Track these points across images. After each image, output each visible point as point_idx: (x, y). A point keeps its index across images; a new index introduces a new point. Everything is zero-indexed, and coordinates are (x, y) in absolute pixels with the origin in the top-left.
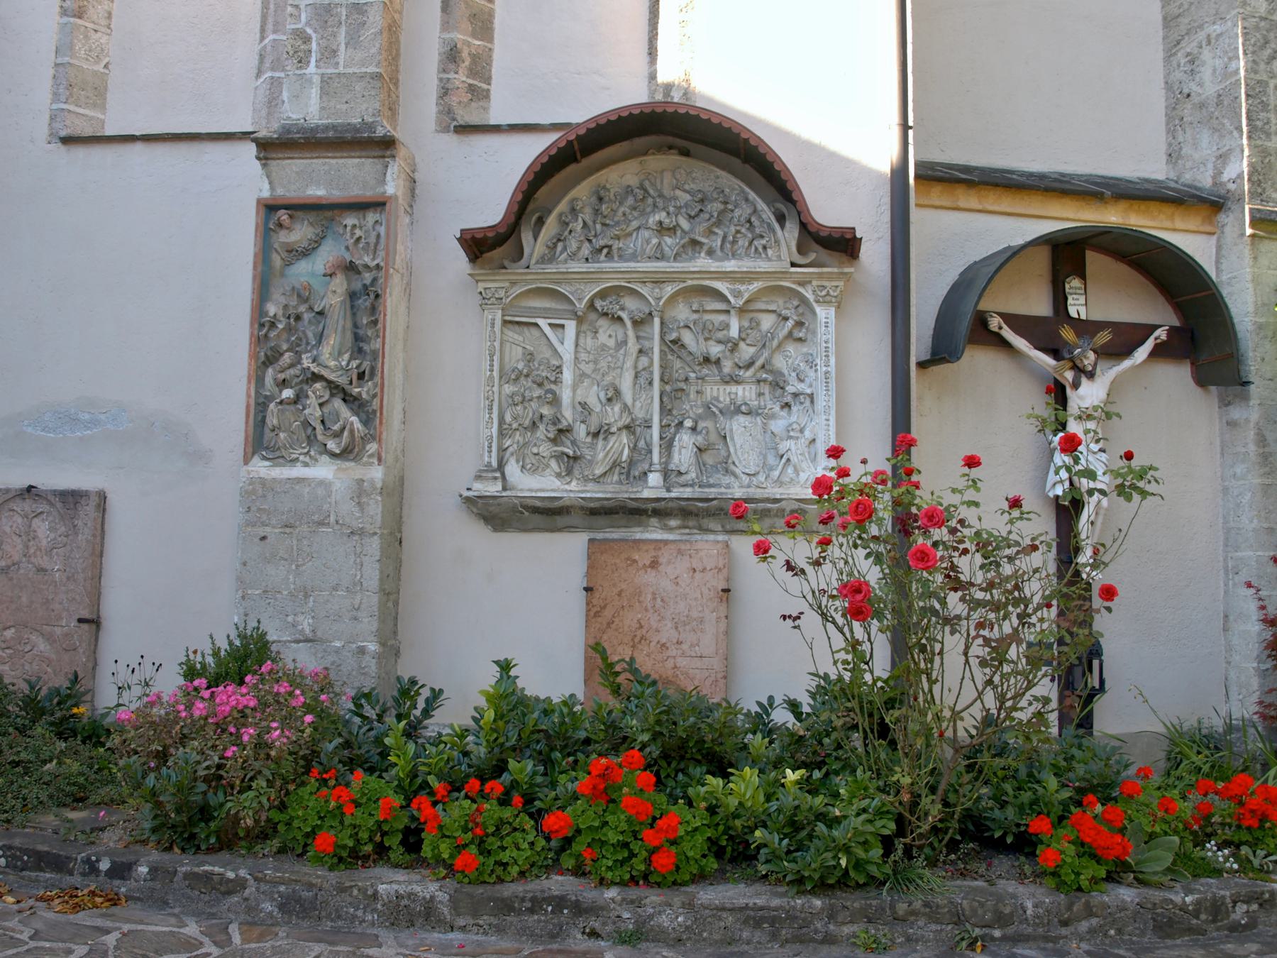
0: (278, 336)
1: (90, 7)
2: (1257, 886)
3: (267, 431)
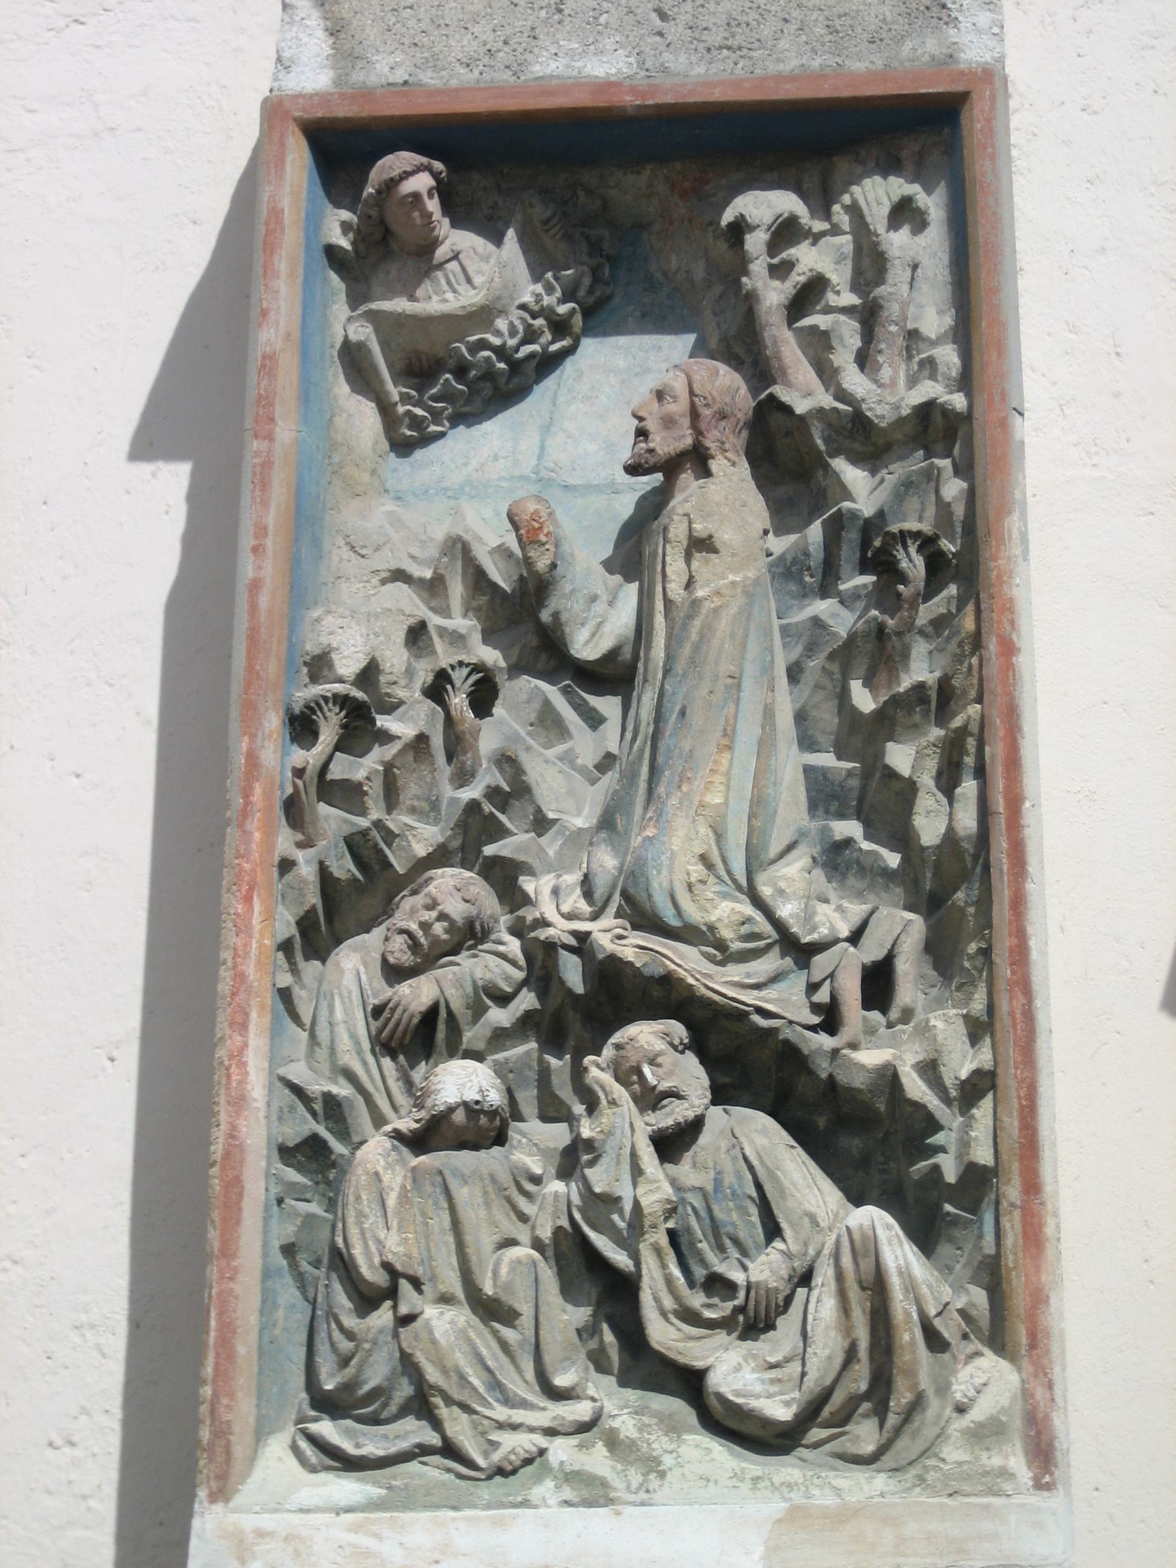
2: (1015, 1245)
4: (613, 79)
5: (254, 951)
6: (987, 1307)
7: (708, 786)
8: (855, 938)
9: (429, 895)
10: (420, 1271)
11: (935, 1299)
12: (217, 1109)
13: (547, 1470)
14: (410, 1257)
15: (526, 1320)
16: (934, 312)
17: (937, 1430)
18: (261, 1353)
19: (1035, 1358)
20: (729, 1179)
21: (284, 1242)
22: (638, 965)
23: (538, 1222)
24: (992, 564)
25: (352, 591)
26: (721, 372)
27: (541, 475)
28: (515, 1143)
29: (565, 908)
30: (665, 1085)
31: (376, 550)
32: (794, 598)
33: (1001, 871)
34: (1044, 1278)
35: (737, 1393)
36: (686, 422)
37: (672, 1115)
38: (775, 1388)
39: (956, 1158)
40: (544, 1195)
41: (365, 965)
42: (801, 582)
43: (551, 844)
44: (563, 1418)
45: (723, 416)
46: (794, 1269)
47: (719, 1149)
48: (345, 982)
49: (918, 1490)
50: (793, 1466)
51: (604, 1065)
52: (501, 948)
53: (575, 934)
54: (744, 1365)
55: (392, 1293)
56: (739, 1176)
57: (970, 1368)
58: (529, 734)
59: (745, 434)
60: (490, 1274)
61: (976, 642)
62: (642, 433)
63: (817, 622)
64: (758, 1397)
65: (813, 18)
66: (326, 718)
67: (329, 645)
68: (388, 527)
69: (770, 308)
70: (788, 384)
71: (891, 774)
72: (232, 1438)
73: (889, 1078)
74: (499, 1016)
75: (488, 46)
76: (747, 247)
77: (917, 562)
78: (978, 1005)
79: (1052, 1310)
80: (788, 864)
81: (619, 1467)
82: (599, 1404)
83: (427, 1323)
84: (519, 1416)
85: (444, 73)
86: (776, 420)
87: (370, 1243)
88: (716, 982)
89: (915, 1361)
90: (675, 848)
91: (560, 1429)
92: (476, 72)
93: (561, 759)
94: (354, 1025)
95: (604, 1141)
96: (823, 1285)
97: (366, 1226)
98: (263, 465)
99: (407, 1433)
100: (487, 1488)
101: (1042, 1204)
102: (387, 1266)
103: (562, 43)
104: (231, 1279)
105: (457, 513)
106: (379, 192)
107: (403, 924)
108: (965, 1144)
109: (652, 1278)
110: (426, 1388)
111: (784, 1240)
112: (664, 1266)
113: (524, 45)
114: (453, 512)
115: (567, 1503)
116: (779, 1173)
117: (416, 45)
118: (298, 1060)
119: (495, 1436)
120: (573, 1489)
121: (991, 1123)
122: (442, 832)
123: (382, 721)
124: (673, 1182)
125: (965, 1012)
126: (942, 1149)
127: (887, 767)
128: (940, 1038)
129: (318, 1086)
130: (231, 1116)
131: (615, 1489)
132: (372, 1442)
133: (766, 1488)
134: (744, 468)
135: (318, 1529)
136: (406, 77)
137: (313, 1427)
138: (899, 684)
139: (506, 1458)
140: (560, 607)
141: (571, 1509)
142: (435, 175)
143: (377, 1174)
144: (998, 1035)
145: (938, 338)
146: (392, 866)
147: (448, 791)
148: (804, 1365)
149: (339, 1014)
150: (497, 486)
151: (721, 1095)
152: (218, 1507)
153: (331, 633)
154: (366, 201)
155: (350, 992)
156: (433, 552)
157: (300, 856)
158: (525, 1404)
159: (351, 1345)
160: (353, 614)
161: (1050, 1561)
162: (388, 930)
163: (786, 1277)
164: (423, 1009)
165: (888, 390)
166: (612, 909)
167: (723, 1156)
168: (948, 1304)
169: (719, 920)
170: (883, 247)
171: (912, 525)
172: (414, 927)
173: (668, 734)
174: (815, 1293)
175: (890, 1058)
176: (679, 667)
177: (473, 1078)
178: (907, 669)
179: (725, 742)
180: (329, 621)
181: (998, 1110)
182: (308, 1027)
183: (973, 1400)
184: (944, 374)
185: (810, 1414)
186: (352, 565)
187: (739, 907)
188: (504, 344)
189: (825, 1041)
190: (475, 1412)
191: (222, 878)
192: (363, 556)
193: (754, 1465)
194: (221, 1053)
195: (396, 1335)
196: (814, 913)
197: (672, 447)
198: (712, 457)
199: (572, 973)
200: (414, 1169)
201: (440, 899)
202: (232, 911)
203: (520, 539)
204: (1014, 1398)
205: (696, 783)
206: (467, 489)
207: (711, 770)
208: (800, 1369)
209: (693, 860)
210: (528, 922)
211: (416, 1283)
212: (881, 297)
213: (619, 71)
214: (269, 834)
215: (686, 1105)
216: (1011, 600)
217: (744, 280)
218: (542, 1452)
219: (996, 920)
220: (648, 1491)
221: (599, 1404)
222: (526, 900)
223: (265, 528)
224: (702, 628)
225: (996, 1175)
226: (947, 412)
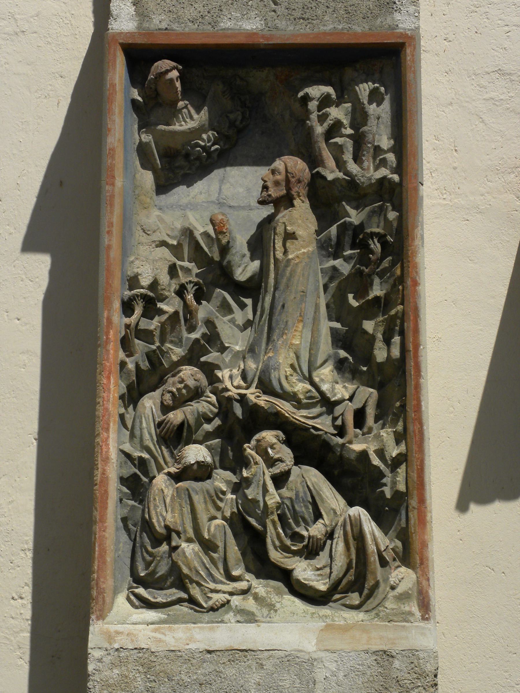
2: (415, 524)
4: (255, 31)
5: (111, 400)
6: (402, 548)
7: (294, 337)
8: (351, 399)
9: (180, 377)
10: (180, 529)
11: (383, 544)
12: (97, 463)
13: (230, 608)
14: (176, 523)
15: (221, 549)
16: (386, 138)
17: (384, 596)
18: (115, 561)
19: (422, 568)
20: (301, 494)
21: (123, 516)
22: (266, 408)
23: (225, 510)
24: (410, 248)
25: (143, 250)
26: (299, 163)
27: (220, 201)
28: (215, 478)
29: (235, 384)
30: (277, 456)
31: (154, 232)
32: (324, 257)
33: (411, 374)
34: (426, 537)
36: (284, 184)
37: (278, 469)
38: (320, 578)
39: (391, 488)
40: (227, 499)
41: (154, 405)
42: (328, 250)
43: (227, 357)
44: (237, 588)
45: (299, 181)
46: (327, 531)
47: (297, 482)
48: (146, 412)
49: (376, 619)
50: (327, 609)
51: (252, 448)
52: (209, 399)
53: (239, 394)
54: (307, 568)
55: (168, 539)
56: (305, 493)
57: (396, 572)
58: (217, 311)
59: (307, 188)
60: (206, 530)
61: (401, 280)
62: (265, 188)
63: (334, 269)
64: (313, 581)
65: (339, 6)
66: (137, 303)
67: (137, 273)
68: (158, 222)
69: (318, 134)
70: (324, 167)
71: (365, 332)
72: (105, 595)
73: (364, 454)
74: (208, 427)
75: (201, 14)
76: (309, 107)
77: (378, 246)
78: (400, 427)
79: (429, 550)
80: (325, 368)
81: (259, 608)
82: (250, 583)
84: (219, 587)
85: (183, 25)
86: (319, 181)
87: (160, 517)
88: (297, 416)
89: (376, 568)
90: (281, 361)
91: (235, 592)
92: (196, 25)
93: (229, 321)
94: (150, 429)
95: (253, 478)
96: (338, 537)
97: (158, 510)
98: (110, 196)
99: (174, 593)
100: (207, 615)
101: (426, 508)
102: (167, 527)
103: (232, 13)
104: (104, 531)
105: (185, 216)
106: (156, 78)
107: (170, 389)
108: (394, 483)
109: (271, 533)
110: (182, 575)
111: (323, 519)
112: (276, 529)
113: (217, 14)
114: (183, 216)
115: (238, 622)
116: (321, 492)
117: (170, 11)
118: (126, 443)
119: (210, 595)
120: (241, 616)
121: (405, 475)
122: (184, 351)
123: (160, 305)
124: (279, 495)
125: (394, 430)
126: (385, 485)
127: (363, 329)
128: (385, 440)
129: (137, 454)
130: (103, 466)
131: (257, 616)
132: (161, 597)
133: (316, 617)
134: (307, 204)
135: (140, 631)
136: (166, 26)
137: (136, 591)
138: (368, 296)
139: (214, 603)
140: (231, 259)
141: (240, 624)
142: (179, 71)
143: (162, 490)
144: (408, 440)
145: (388, 150)
146: (164, 364)
147: (185, 334)
148: (331, 569)
149: (144, 425)
150: (201, 205)
151: (298, 462)
152: (100, 622)
153: (138, 268)
154: (149, 81)
155: (148, 416)
156: (177, 233)
157: (127, 360)
158: (222, 583)
159: (151, 558)
160: (147, 259)
161: (428, 648)
162: (163, 391)
163: (324, 534)
164: (178, 423)
165: (366, 172)
166: (254, 385)
167: (299, 485)
168: (388, 546)
169: (298, 391)
170: (367, 110)
171: (377, 230)
172: (175, 390)
173: (277, 314)
174: (335, 541)
175: (365, 448)
176: (282, 287)
177: (200, 452)
178: (372, 289)
179: (300, 318)
180: (137, 262)
181: (408, 470)
182: (130, 426)
183: (398, 584)
184: (390, 166)
185: (334, 588)
186: (144, 238)
187: (305, 385)
188: (206, 145)
189: (340, 441)
190: (203, 586)
191: (97, 369)
192: (148, 235)
193: (311, 609)
194: (98, 440)
195: (170, 556)
196: (335, 388)
197: (278, 194)
198: (295, 199)
199: (238, 410)
200: (177, 488)
201: (185, 379)
202: (102, 382)
203: (215, 230)
204: (414, 584)
205: (289, 335)
206: (189, 206)
207: (295, 330)
208: (329, 570)
209: (289, 366)
210: (220, 389)
211: (178, 534)
212: (365, 132)
213: (257, 28)
214: (116, 351)
215: (285, 464)
216: (416, 263)
217: (308, 122)
218: (228, 602)
219: (408, 394)
220: (270, 617)
221: (250, 583)
222: (219, 380)
223: (112, 223)
224: (291, 271)
225: (407, 496)
226: (390, 181)
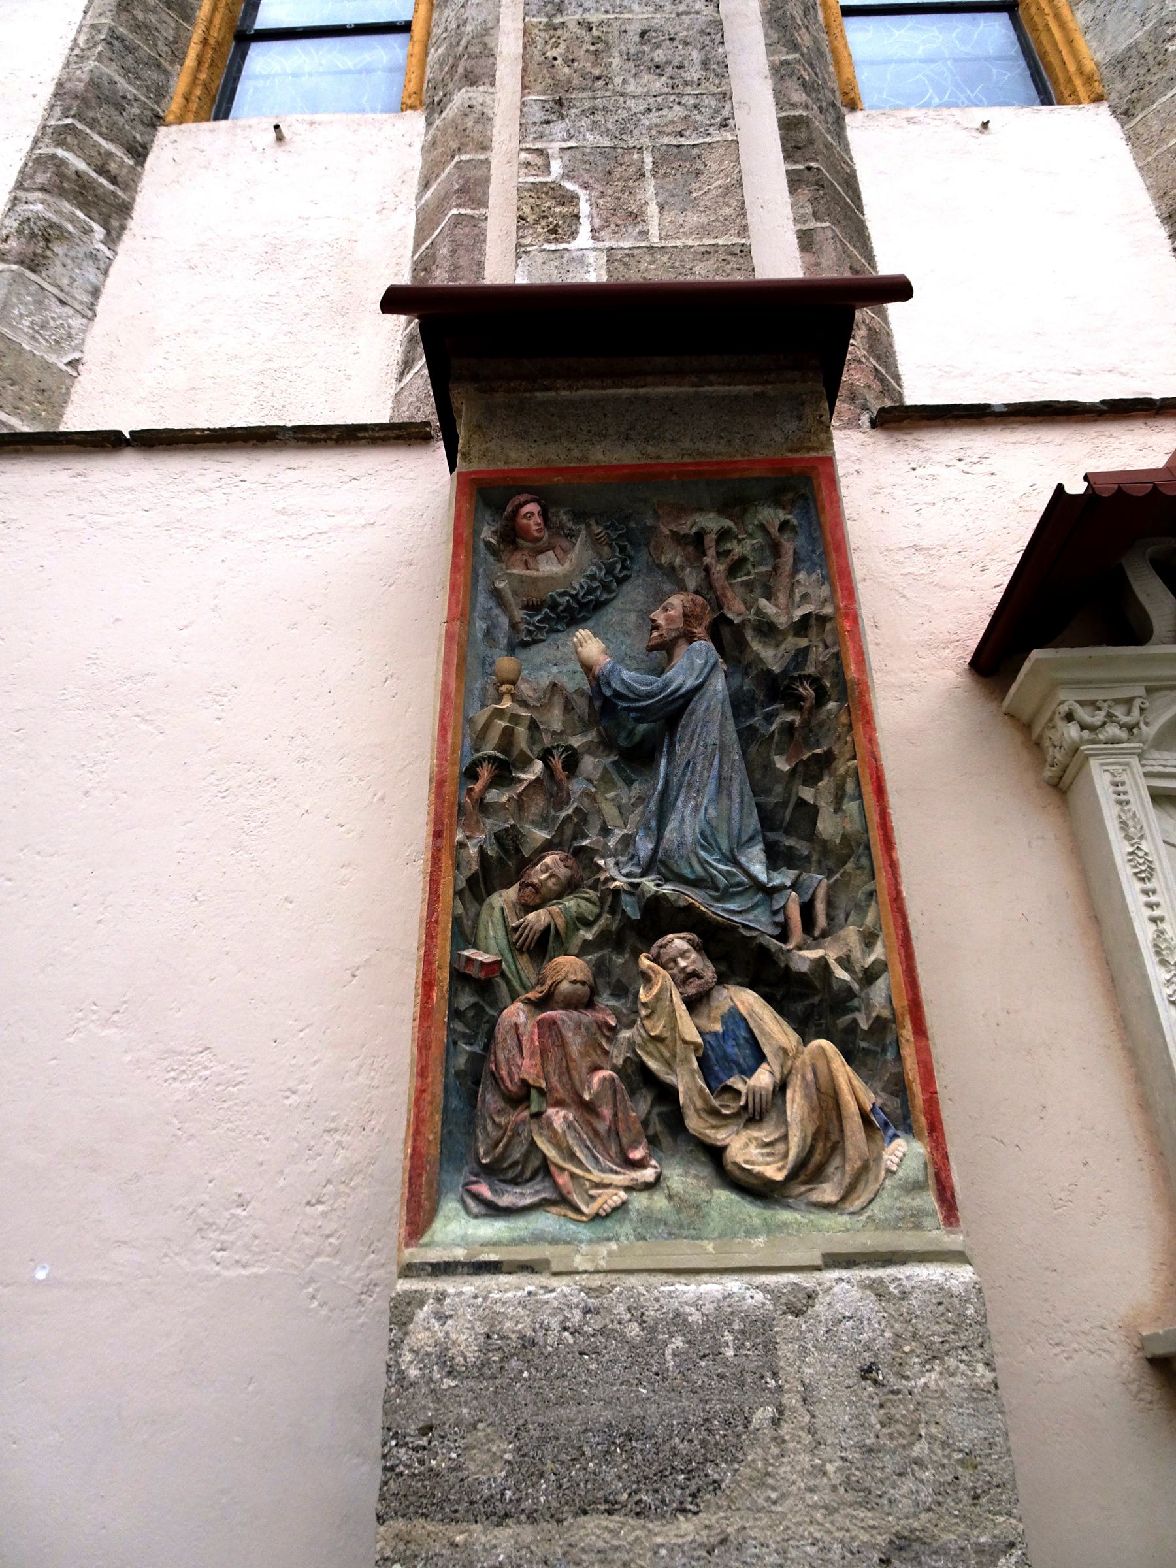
0: (520, 803)
1: (58, 263)
3: (491, 1100)
35: (747, 1162)
38: (769, 1159)
53: (631, 884)
64: (759, 1164)
73: (822, 965)
83: (549, 1118)
137: (475, 1188)
185: (793, 1176)
